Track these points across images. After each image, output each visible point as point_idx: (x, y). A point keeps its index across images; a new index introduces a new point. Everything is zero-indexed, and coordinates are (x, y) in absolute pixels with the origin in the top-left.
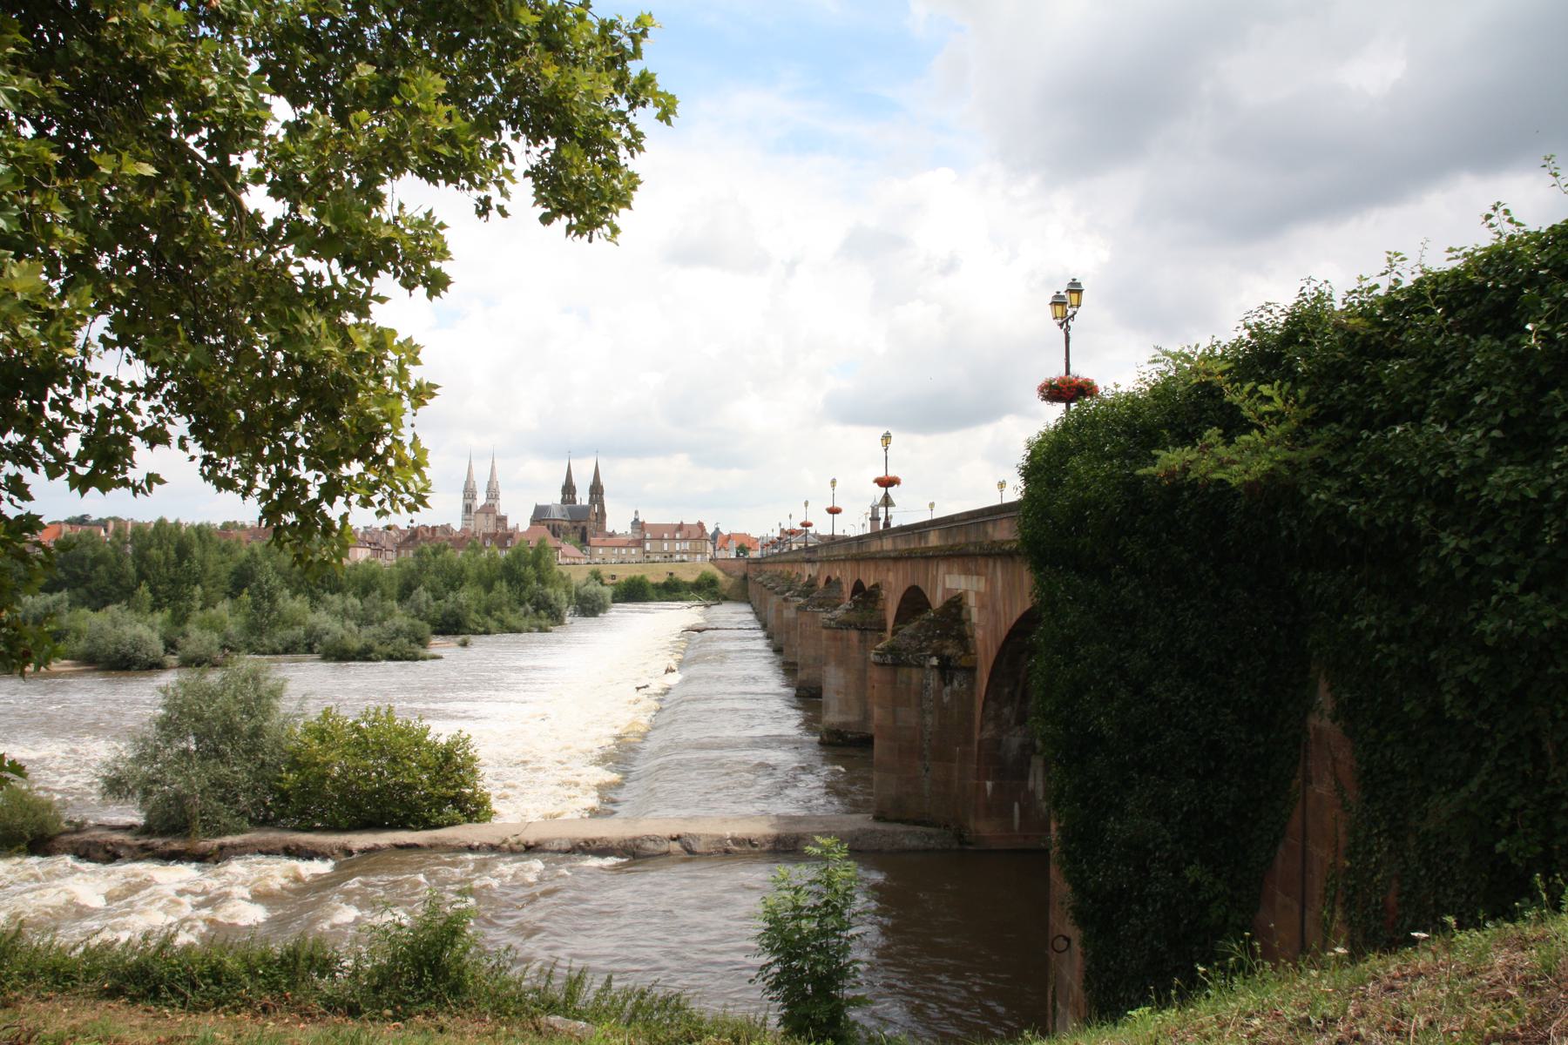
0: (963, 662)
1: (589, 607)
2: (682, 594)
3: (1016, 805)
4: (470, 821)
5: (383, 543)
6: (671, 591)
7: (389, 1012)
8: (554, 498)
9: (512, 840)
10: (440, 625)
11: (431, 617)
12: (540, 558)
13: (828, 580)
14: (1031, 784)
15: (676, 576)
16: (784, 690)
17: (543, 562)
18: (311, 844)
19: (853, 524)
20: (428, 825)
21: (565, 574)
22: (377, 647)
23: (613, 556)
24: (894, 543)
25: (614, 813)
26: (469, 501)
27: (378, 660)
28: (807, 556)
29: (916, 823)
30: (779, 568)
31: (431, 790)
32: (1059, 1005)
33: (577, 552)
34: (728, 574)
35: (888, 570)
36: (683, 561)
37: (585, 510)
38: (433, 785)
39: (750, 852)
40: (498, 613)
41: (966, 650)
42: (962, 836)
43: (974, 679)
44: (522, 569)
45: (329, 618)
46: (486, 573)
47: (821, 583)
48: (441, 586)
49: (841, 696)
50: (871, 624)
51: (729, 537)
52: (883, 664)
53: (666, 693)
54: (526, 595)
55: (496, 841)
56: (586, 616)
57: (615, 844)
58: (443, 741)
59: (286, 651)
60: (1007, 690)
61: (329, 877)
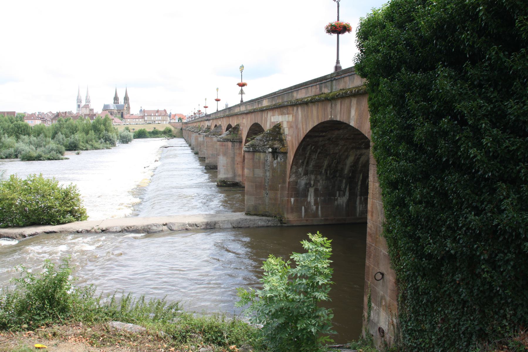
0: (282, 150)
1: (125, 140)
2: (159, 135)
3: (303, 208)
4: (78, 220)
5: (46, 118)
6: (155, 134)
7: (26, 326)
8: (110, 102)
9: (96, 228)
10: (69, 147)
11: (65, 144)
12: (106, 122)
13: (216, 126)
14: (309, 199)
15: (156, 129)
16: (201, 167)
17: (107, 123)
18: (7, 233)
19: (225, 108)
20: (59, 223)
21: (116, 128)
22: (43, 155)
23: (133, 122)
24: (246, 107)
25: (138, 215)
26: (79, 103)
27: (44, 160)
28: (207, 118)
29: (263, 216)
30: (195, 124)
31: (60, 208)
32: (373, 305)
33: (120, 121)
34: (176, 128)
35: (243, 118)
36: (159, 123)
37: (123, 106)
38: (61, 206)
39: (196, 230)
40: (91, 142)
41: (283, 145)
42: (281, 220)
43: (286, 157)
44: (100, 126)
45: (24, 145)
46: (86, 128)
47: (213, 128)
48: (69, 133)
49: (225, 167)
50: (236, 139)
51: (175, 115)
52: (249, 152)
53: (156, 169)
54: (101, 136)
55: (89, 229)
56: (124, 143)
57: (140, 228)
58: (64, 187)
59: (7, 158)
60: (301, 161)
61: (16, 246)
